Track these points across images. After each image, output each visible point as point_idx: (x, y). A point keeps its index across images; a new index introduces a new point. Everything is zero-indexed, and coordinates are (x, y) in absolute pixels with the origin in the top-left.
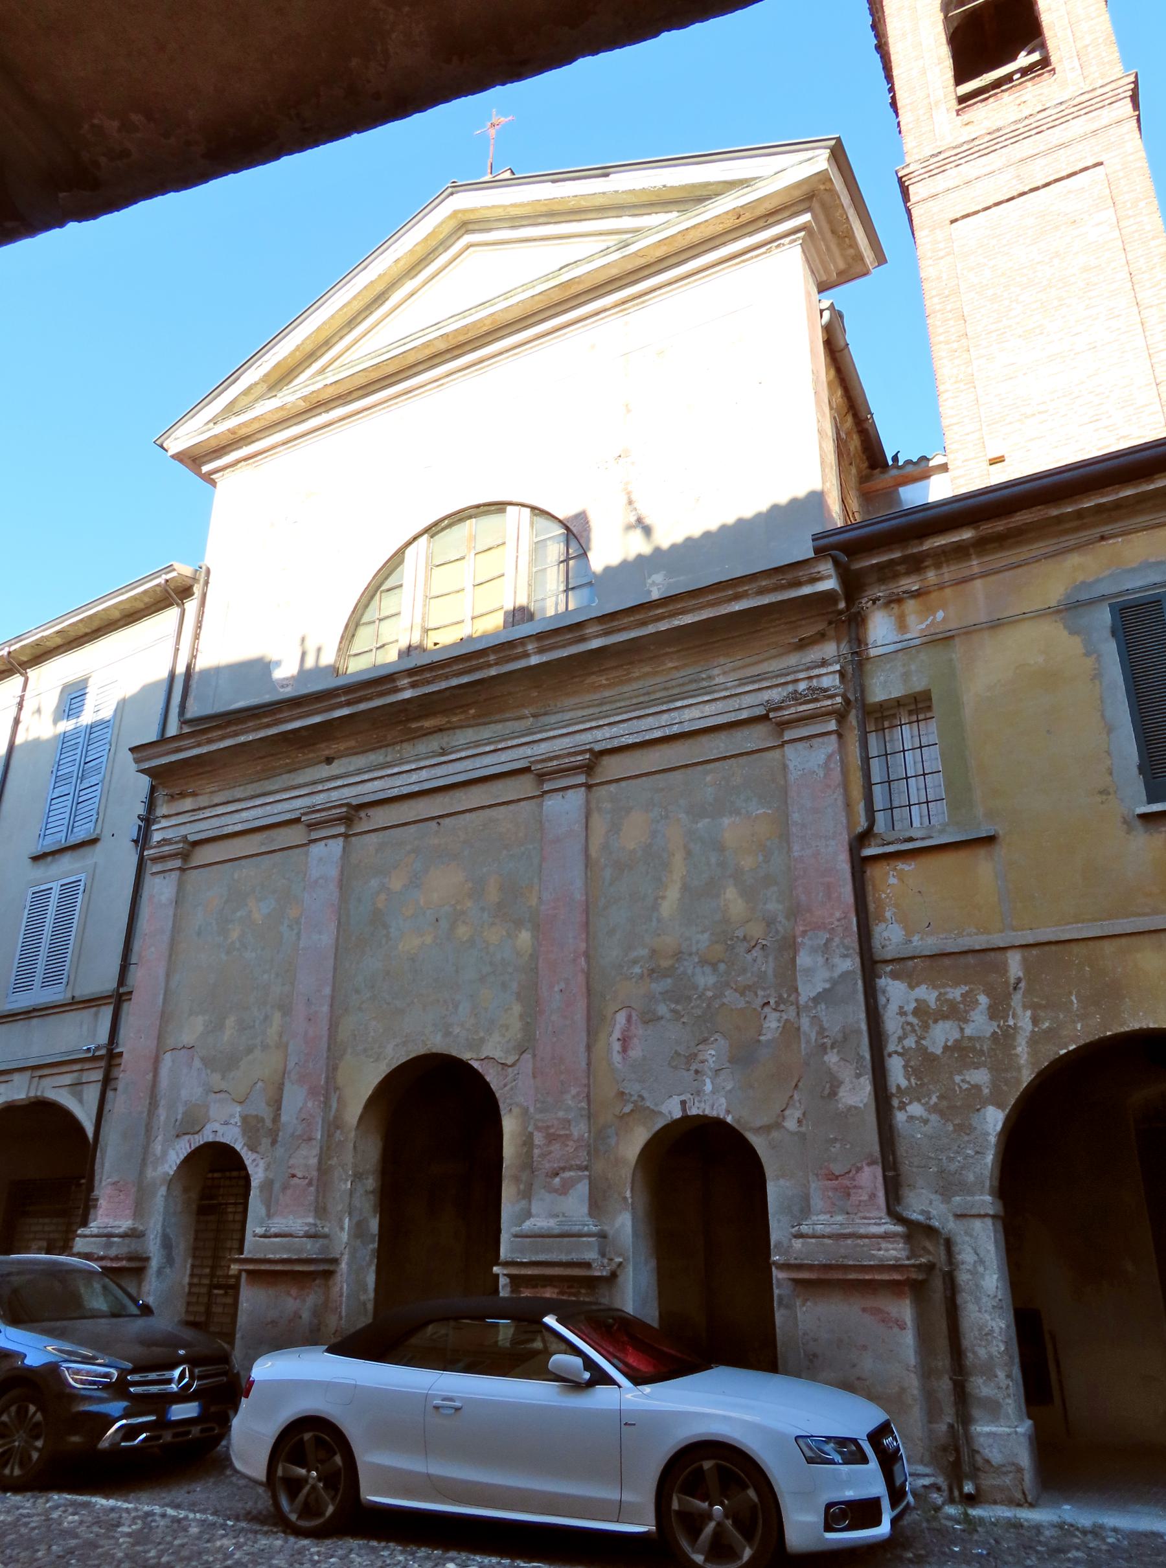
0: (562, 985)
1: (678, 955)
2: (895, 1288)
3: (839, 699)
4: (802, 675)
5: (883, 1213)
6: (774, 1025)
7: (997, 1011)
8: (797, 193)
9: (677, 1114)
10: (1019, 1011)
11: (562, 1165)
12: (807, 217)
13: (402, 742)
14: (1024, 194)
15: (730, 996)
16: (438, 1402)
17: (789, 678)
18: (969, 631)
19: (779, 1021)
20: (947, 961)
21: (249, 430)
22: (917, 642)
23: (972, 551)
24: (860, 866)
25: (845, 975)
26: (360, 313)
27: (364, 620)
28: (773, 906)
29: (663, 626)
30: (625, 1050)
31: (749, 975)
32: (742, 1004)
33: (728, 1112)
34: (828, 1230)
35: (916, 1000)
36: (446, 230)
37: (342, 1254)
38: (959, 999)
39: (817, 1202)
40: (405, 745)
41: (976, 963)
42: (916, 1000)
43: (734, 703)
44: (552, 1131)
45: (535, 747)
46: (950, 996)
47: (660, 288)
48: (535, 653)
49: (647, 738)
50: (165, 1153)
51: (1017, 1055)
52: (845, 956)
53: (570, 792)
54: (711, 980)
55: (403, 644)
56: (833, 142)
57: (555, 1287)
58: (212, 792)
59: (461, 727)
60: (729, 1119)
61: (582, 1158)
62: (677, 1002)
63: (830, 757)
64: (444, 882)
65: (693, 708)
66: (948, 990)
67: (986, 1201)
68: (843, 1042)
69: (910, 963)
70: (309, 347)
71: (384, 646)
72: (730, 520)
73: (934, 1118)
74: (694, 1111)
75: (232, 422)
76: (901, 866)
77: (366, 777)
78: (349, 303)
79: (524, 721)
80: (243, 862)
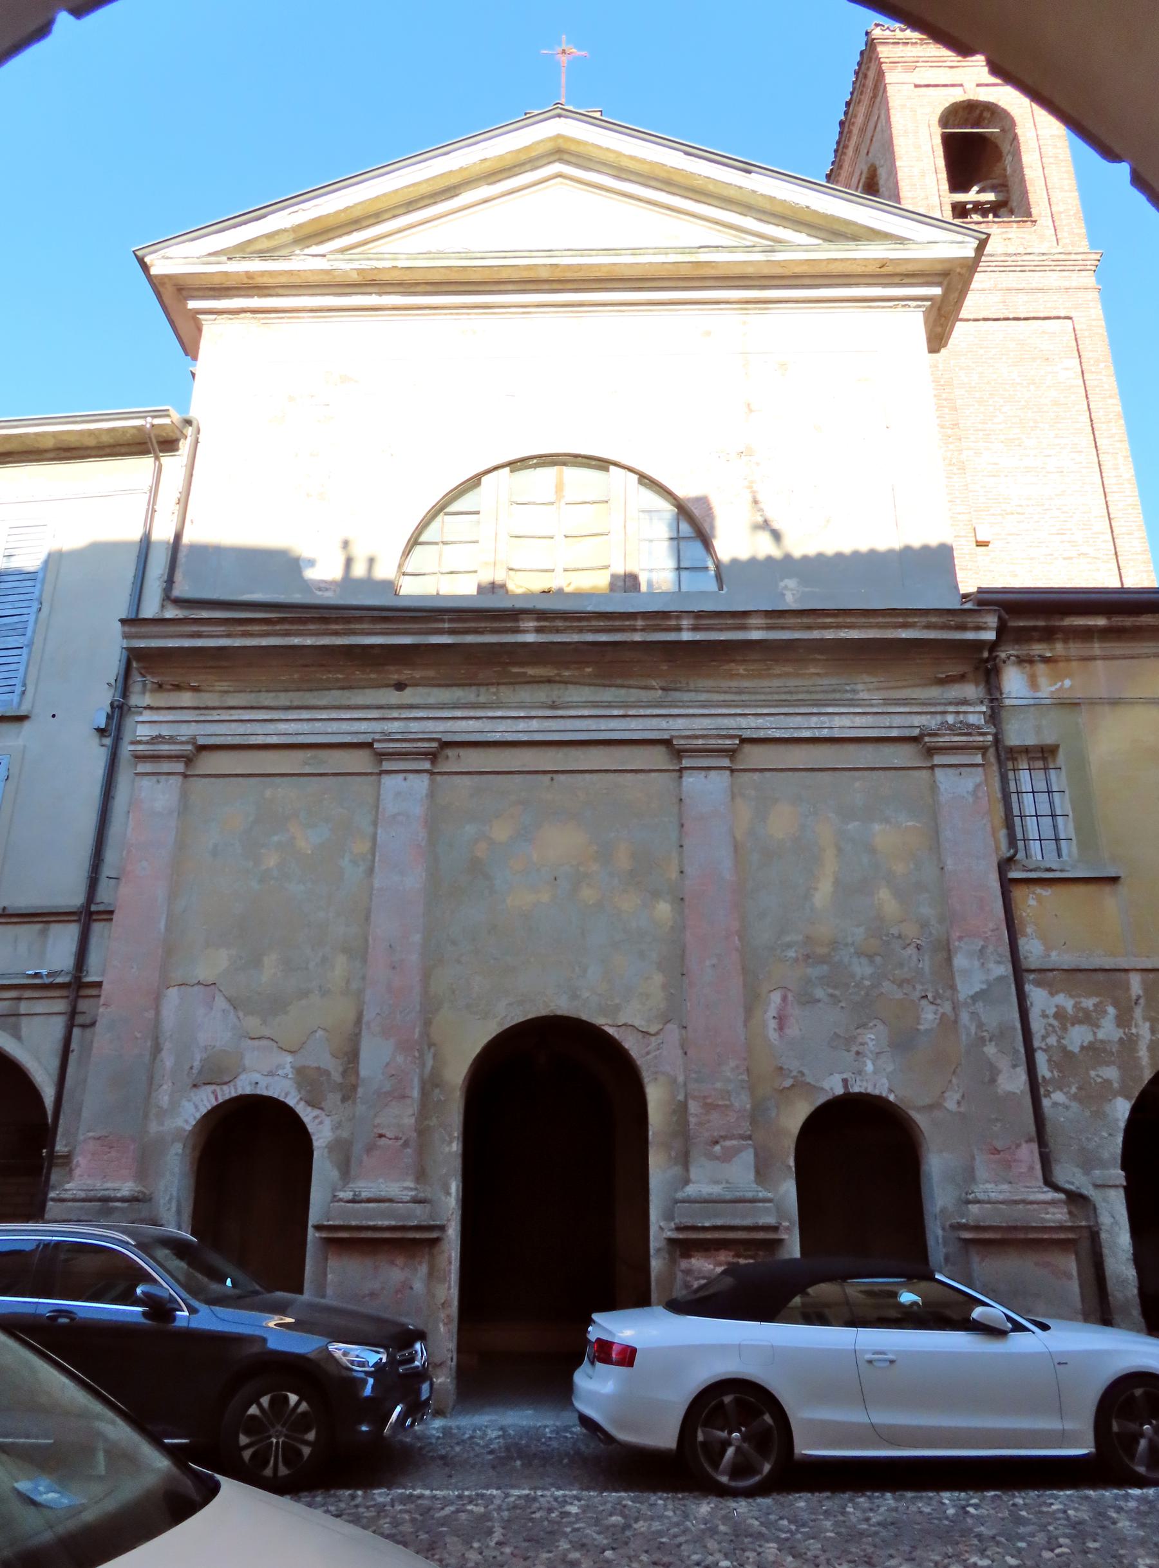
0: (715, 961)
1: (835, 944)
2: (1064, 1245)
3: (990, 738)
4: (951, 709)
5: (1041, 1183)
6: (931, 1016)
7: (1123, 1020)
8: (939, 267)
9: (839, 1091)
10: (1140, 1022)
11: (722, 1133)
12: (937, 291)
13: (499, 684)
14: (1008, 319)
15: (887, 987)
16: (868, 1356)
17: (939, 709)
18: (1093, 702)
19: (935, 1013)
20: (1080, 976)
21: (271, 280)
22: (1048, 701)
23: (1096, 635)
24: (1007, 885)
25: (1001, 979)
26: (422, 198)
27: (422, 539)
28: (926, 911)
29: (829, 635)
30: (781, 1028)
31: (906, 969)
32: (899, 995)
33: (891, 1091)
34: (1001, 1197)
35: (1057, 1006)
36: (541, 150)
37: (449, 1220)
38: (1091, 1008)
39: (981, 1172)
40: (502, 688)
41: (1103, 980)
42: (1057, 1006)
43: (886, 721)
44: (709, 1101)
45: (671, 721)
46: (1084, 1005)
47: (787, 302)
48: (688, 629)
49: (796, 735)
50: (175, 1105)
51: (1139, 1058)
52: (999, 963)
53: (713, 773)
54: (868, 970)
55: (486, 577)
56: (984, 236)
57: (730, 1250)
58: (226, 692)
59: (575, 683)
60: (892, 1098)
61: (745, 1127)
62: (835, 987)
63: (978, 786)
64: (562, 843)
65: (843, 717)
66: (1082, 999)
67: (1118, 1175)
68: (999, 1036)
69: (1050, 974)
70: (358, 213)
71: (445, 575)
72: (864, 548)
73: (1075, 1105)
74: (856, 1089)
75: (255, 266)
76: (1039, 890)
77: (459, 713)
78: (419, 183)
79: (652, 692)
80: (278, 780)
